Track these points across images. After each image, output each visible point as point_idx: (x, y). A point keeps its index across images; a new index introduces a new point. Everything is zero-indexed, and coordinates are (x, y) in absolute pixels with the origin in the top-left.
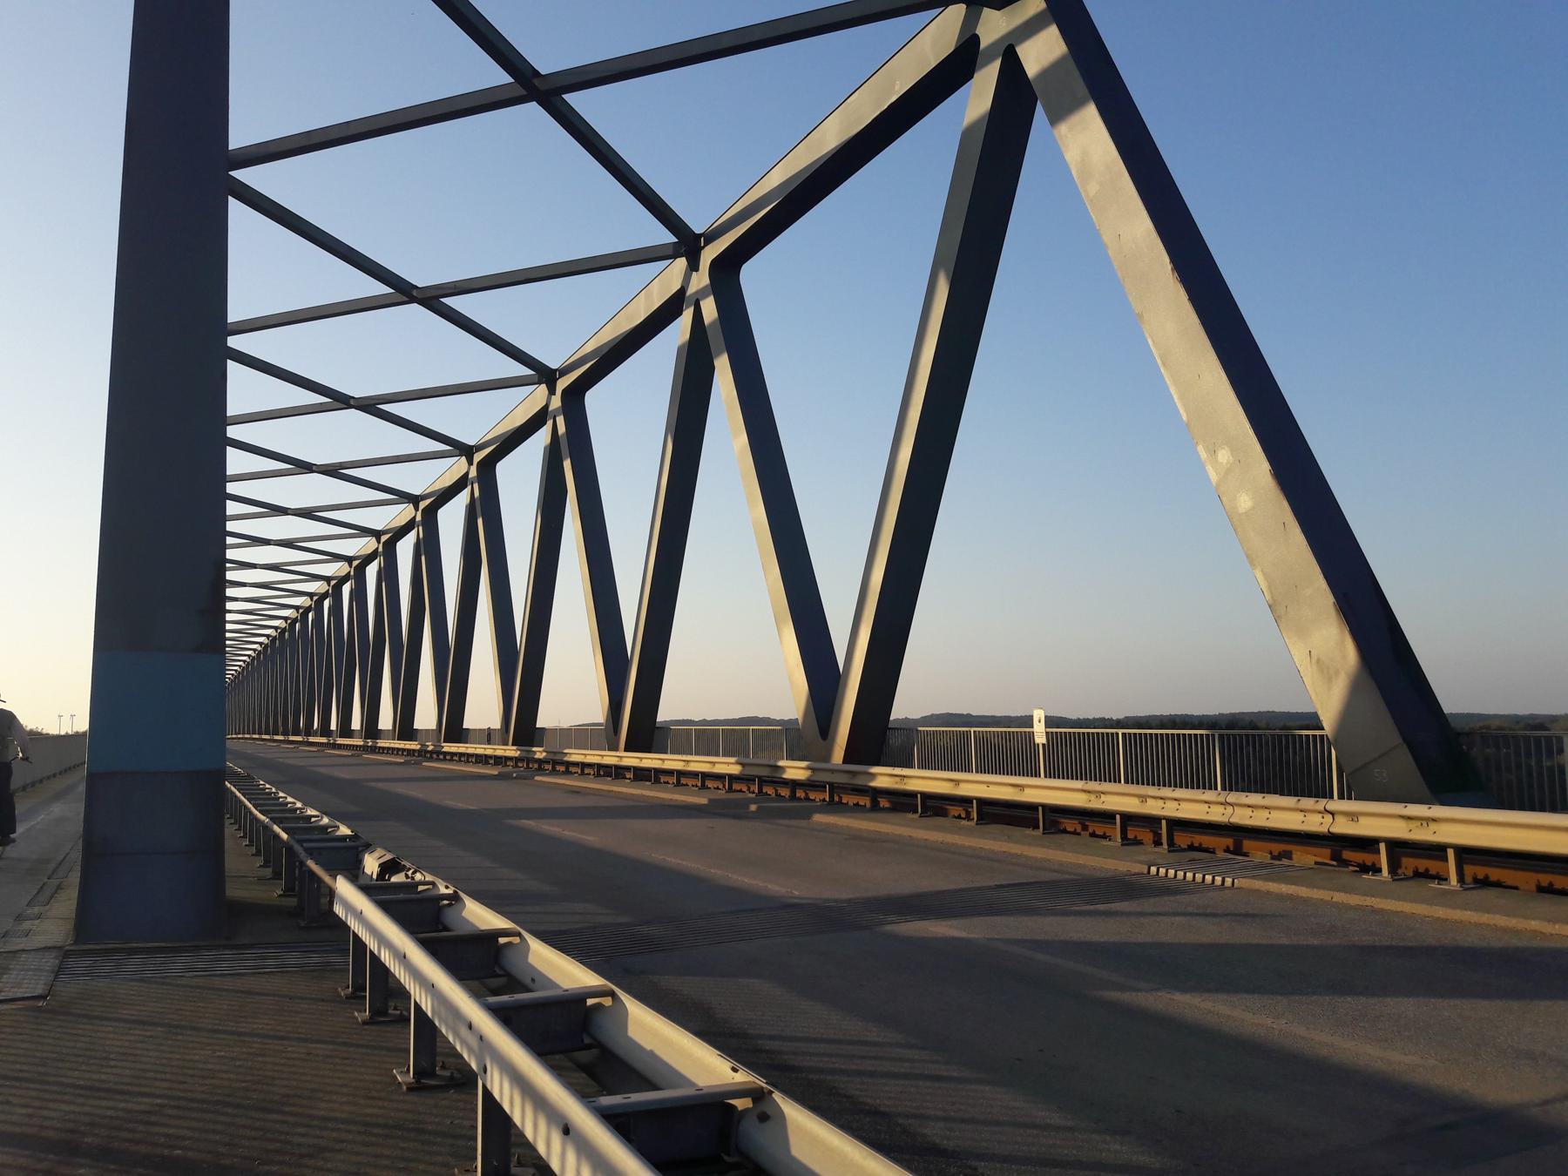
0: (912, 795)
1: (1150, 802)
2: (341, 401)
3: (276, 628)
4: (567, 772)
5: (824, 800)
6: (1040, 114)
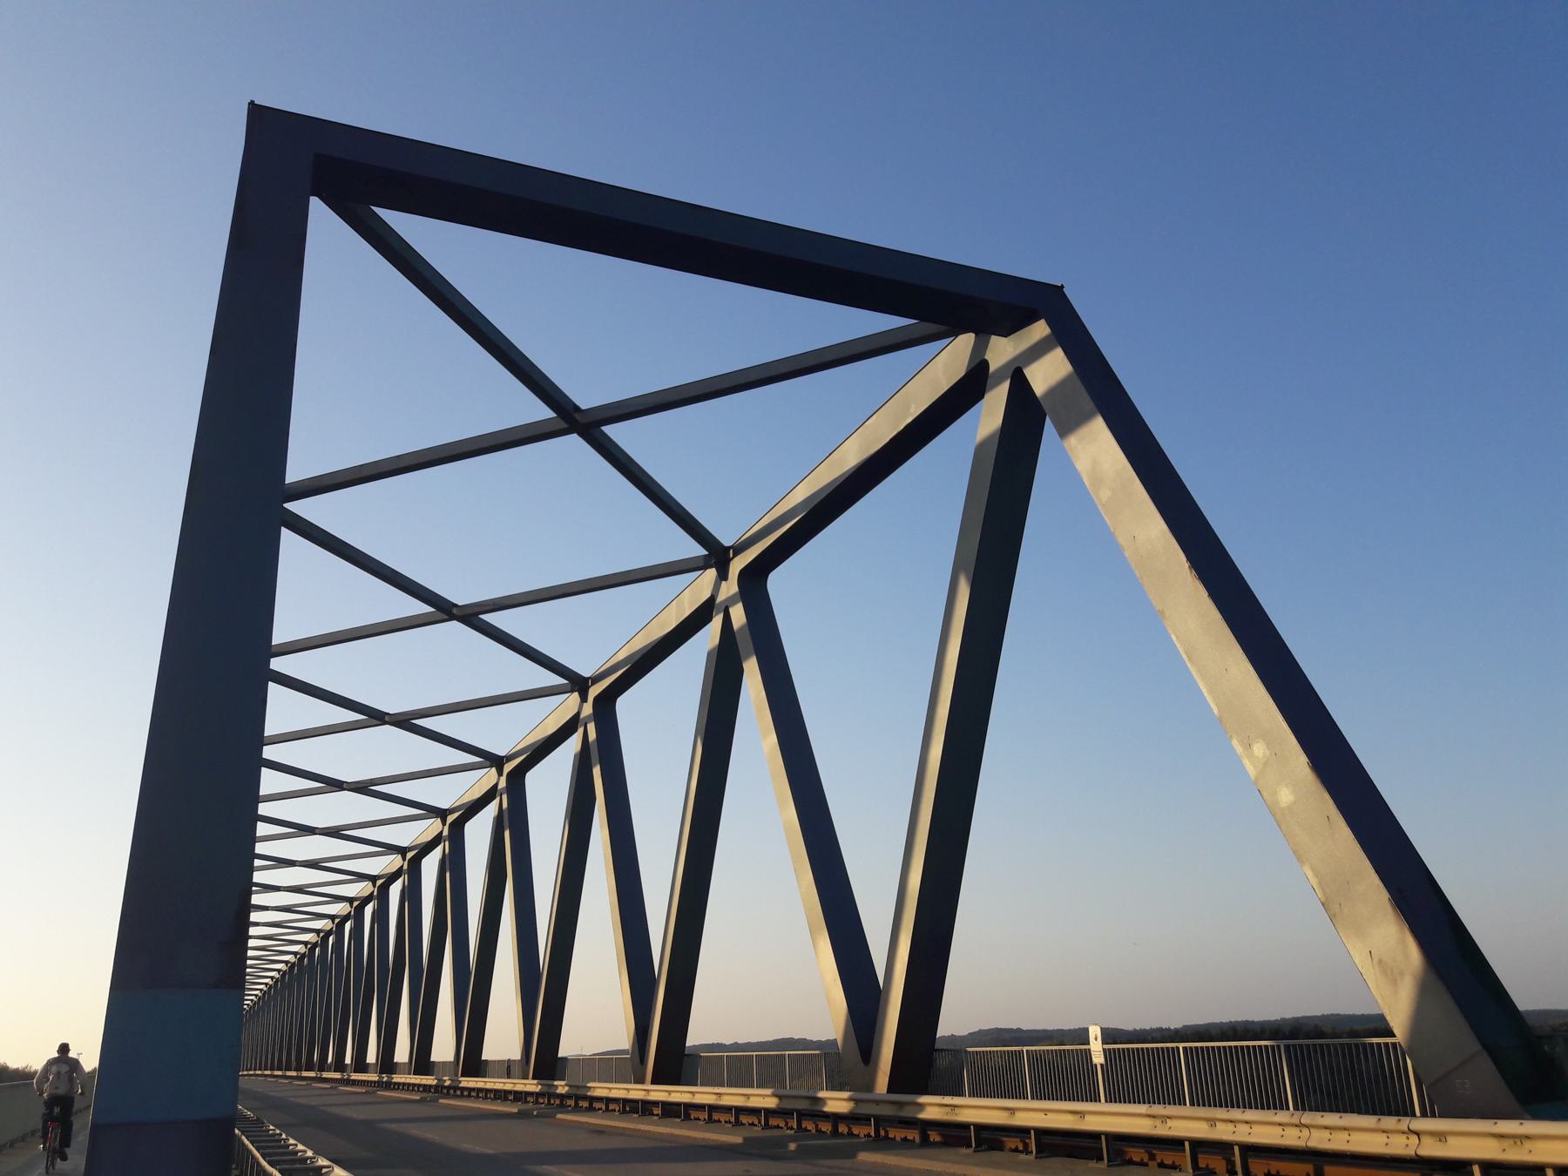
0: (965, 1126)
1: (1220, 1126)
2: (376, 717)
3: (295, 954)
4: (591, 1109)
5: (869, 1135)
6: (1049, 428)
